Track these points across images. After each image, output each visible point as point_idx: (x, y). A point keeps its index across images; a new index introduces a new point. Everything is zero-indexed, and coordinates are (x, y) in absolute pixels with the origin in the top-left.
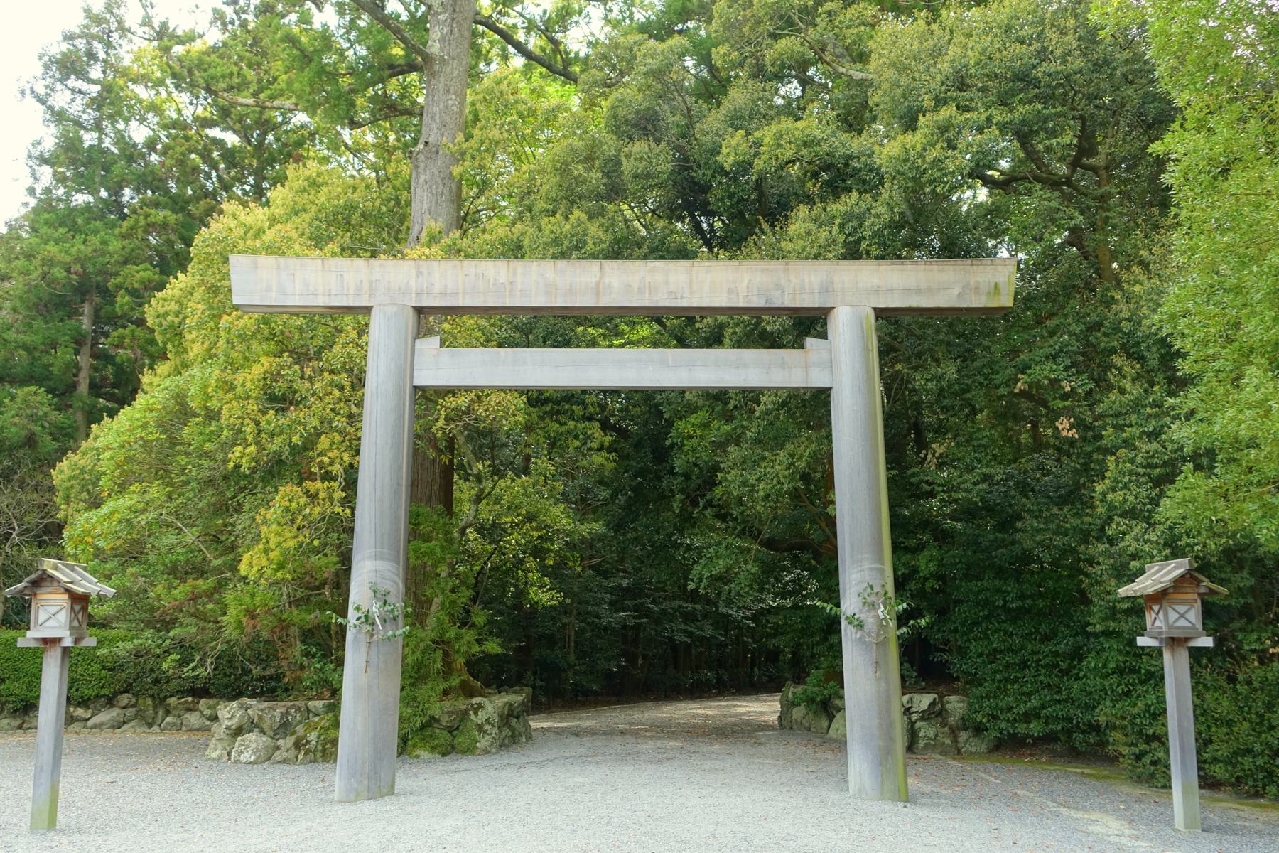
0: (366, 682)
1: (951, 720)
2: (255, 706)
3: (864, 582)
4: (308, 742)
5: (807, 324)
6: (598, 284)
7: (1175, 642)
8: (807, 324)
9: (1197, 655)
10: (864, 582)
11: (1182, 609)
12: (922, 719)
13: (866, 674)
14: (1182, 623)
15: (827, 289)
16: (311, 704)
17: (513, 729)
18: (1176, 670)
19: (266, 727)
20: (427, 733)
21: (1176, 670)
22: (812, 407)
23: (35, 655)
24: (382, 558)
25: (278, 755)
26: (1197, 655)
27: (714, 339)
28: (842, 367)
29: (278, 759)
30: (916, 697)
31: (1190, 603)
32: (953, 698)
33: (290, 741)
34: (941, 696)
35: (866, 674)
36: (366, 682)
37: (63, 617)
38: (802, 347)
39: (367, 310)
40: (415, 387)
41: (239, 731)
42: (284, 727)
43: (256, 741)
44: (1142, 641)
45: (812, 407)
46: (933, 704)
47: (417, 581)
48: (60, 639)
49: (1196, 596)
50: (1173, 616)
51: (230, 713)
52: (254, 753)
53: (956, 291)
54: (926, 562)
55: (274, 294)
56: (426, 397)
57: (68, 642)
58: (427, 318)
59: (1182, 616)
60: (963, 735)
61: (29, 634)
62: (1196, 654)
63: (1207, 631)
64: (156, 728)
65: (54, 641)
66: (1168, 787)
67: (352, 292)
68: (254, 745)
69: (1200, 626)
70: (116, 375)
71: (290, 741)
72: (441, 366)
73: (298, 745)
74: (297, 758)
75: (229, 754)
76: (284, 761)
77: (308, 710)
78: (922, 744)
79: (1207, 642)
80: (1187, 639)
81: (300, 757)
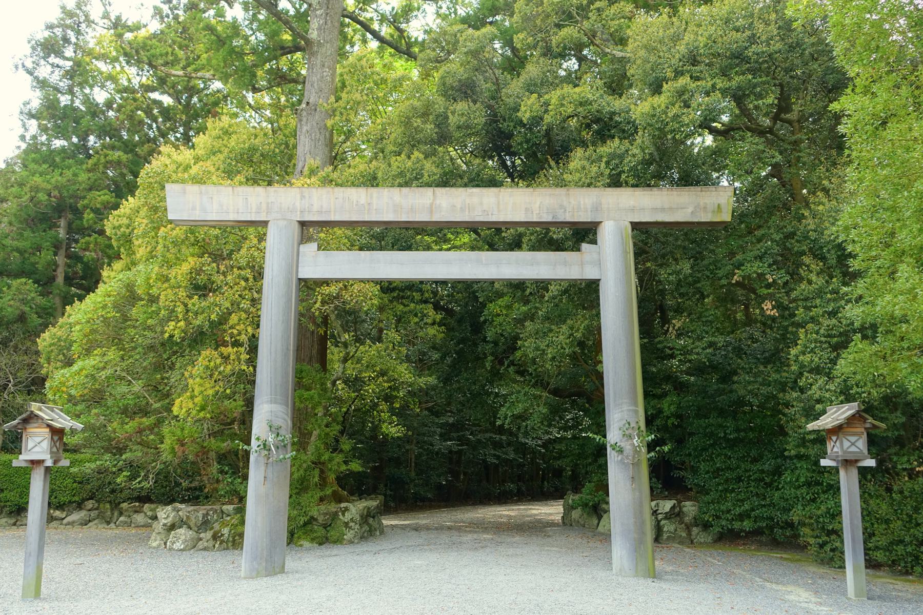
0: (264, 491)
1: (687, 519)
2: (184, 509)
3: (623, 420)
4: (222, 535)
5: (583, 234)
6: (431, 205)
7: (848, 463)
8: (583, 234)
9: (864, 472)
10: (623, 420)
11: (853, 439)
12: (666, 518)
13: (625, 486)
14: (853, 449)
15: (597, 208)
16: (225, 507)
17: (370, 526)
18: (848, 483)
19: (192, 524)
20: (308, 529)
21: (848, 483)
22: (586, 293)
23: (25, 473)
24: (276, 403)
25: (201, 545)
26: (864, 472)
27: (515, 245)
28: (608, 264)
29: (201, 547)
30: (661, 502)
31: (859, 435)
32: (688, 503)
33: (209, 534)
34: (679, 502)
35: (625, 486)
36: (264, 491)
37: (46, 445)
38: (579, 250)
39: (265, 224)
40: (300, 279)
41: (172, 527)
42: (205, 524)
43: (185, 534)
44: (824, 462)
45: (586, 293)
46: (673, 508)
47: (301, 419)
48: (43, 461)
49: (863, 430)
50: (846, 444)
51: (166, 514)
52: (183, 543)
53: (690, 210)
54: (668, 405)
55: (197, 212)
56: (307, 286)
57: (49, 463)
58: (308, 229)
59: (853, 444)
60: (695, 530)
61: (21, 457)
62: (863, 471)
63: (871, 455)
64: (112, 525)
65: (39, 462)
66: (843, 567)
67: (254, 210)
68: (183, 537)
69: (866, 452)
70: (84, 270)
71: (209, 534)
72: (318, 264)
73: (215, 537)
74: (214, 546)
75: (165, 544)
76: (205, 549)
77: (222, 512)
78: (665, 536)
79: (871, 463)
80: (857, 461)
81: (217, 546)
